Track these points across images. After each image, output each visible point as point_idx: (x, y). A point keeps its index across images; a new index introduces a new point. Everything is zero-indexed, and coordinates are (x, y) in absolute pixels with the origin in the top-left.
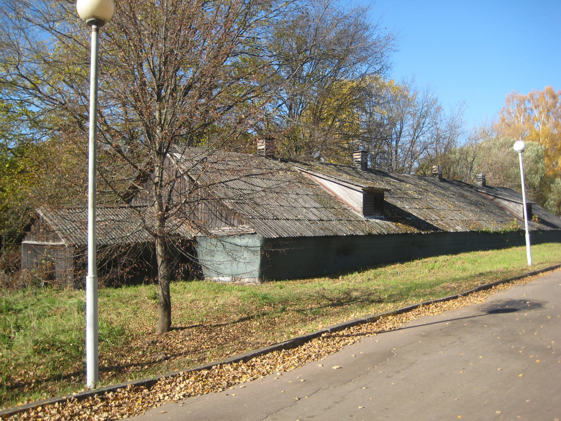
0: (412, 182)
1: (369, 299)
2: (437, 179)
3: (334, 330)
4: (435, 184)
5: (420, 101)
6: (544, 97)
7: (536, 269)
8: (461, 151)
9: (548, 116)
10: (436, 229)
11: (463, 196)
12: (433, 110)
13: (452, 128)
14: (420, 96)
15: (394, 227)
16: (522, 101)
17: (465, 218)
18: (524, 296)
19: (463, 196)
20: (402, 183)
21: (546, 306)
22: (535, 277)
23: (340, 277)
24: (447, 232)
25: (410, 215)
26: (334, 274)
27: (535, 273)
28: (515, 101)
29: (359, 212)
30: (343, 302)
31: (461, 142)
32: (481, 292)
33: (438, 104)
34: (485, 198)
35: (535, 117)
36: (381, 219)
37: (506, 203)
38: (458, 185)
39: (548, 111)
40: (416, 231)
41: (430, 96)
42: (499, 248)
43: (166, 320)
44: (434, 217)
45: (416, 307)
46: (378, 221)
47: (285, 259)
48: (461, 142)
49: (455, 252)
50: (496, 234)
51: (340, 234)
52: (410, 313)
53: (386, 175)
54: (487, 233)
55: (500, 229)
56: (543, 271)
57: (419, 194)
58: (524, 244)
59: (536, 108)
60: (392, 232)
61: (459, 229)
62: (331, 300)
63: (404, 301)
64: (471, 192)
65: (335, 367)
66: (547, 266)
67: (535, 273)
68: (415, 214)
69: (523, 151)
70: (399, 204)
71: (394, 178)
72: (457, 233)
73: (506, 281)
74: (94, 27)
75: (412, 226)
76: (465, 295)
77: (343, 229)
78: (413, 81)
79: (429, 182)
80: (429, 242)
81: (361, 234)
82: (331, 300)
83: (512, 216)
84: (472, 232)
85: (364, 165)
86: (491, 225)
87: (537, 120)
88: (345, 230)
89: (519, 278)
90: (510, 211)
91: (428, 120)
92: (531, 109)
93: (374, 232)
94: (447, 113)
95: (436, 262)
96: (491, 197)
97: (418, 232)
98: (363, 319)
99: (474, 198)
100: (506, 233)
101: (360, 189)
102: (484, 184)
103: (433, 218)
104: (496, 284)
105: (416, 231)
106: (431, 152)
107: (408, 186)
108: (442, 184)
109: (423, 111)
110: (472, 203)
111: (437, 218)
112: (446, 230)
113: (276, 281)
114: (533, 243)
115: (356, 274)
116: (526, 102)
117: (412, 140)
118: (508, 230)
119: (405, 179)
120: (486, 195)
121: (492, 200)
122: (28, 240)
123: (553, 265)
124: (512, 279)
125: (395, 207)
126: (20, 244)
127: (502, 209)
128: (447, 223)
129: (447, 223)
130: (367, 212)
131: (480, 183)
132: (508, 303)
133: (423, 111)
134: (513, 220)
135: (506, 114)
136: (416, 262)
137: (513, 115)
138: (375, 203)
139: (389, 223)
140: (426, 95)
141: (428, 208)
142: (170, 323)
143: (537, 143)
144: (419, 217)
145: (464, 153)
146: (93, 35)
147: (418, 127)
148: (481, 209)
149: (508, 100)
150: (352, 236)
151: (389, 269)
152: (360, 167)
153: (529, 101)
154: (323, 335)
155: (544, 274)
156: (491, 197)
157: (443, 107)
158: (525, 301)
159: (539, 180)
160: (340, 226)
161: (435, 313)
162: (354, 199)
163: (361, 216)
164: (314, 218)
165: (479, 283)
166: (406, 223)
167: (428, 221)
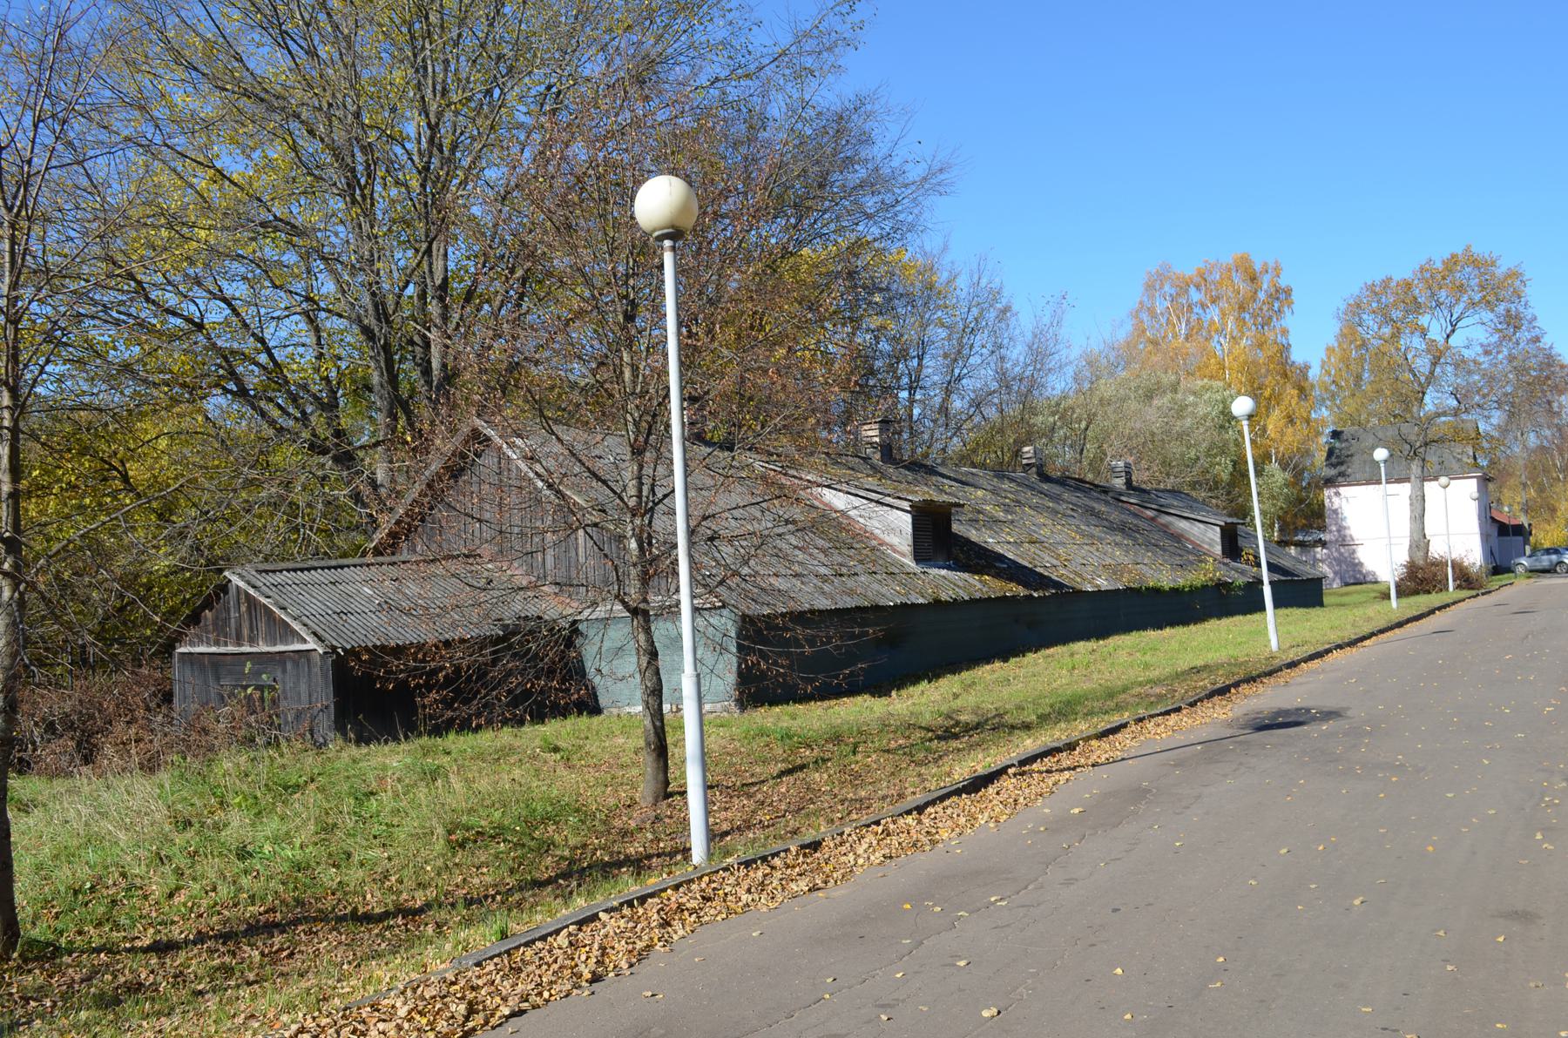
0: (985, 484)
1: (995, 726)
2: (1034, 477)
3: (1023, 763)
4: (1033, 489)
5: (963, 295)
6: (1230, 278)
7: (1292, 656)
8: (1055, 408)
9: (1241, 321)
10: (1058, 585)
11: (1097, 515)
12: (992, 315)
13: (1039, 355)
14: (962, 282)
15: (979, 586)
16: (1183, 286)
17: (1109, 561)
18: (1298, 702)
19: (1097, 515)
20: (967, 488)
21: (1349, 713)
22: (1294, 672)
23: (894, 693)
24: (1081, 591)
25: (1001, 558)
26: (879, 686)
27: (1293, 665)
28: (1167, 288)
29: (904, 555)
30: (951, 732)
31: (1057, 385)
32: (1216, 699)
33: (1004, 301)
34: (1136, 515)
35: (1212, 322)
36: (949, 568)
37: (1183, 524)
38: (1077, 489)
39: (1242, 308)
40: (1022, 591)
41: (984, 282)
42: (1185, 622)
43: (661, 776)
44: (1048, 560)
45: (1124, 726)
46: (944, 572)
47: (786, 658)
48: (1057, 385)
49: (1102, 634)
50: (1175, 591)
51: (883, 602)
52: (1119, 736)
53: (931, 471)
54: (1157, 591)
55: (1181, 582)
56: (1306, 660)
57: (1007, 512)
58: (1262, 608)
59: (1213, 302)
60: (978, 595)
61: (1103, 583)
62: (928, 730)
63: (1115, 712)
64: (1107, 503)
65: (1076, 811)
66: (1312, 651)
67: (1293, 665)
68: (1010, 556)
69: (1250, 417)
70: (973, 535)
71: (949, 478)
72: (1100, 594)
73: (1250, 680)
74: (667, 243)
75: (1011, 580)
76: (1193, 704)
77: (884, 590)
78: (945, 248)
79: (1019, 484)
80: (1047, 615)
81: (921, 601)
82: (928, 730)
83: (1199, 554)
84: (1129, 590)
85: (887, 451)
86: (1164, 576)
87: (1217, 331)
88: (890, 594)
89: (1270, 674)
90: (1192, 542)
91: (979, 339)
92: (1203, 306)
93: (944, 597)
94: (1024, 322)
95: (1072, 655)
96: (1150, 513)
97: (1027, 592)
98: (1056, 745)
99: (1115, 516)
100: (1194, 591)
101: (906, 505)
102: (1129, 483)
103: (1043, 563)
104: (1237, 685)
105: (1022, 591)
106: (991, 412)
107: (980, 493)
108: (1045, 486)
109: (971, 318)
110: (1112, 528)
111: (1055, 562)
112: (1078, 587)
113: (771, 705)
114: (1278, 604)
115: (924, 685)
116: (1192, 290)
117: (950, 388)
118: (1198, 583)
119: (970, 479)
120: (1133, 506)
121: (1153, 519)
122: (192, 644)
123: (1321, 648)
124: (1259, 676)
125: (968, 541)
126: (171, 655)
127: (1178, 538)
128: (1075, 573)
129: (1075, 573)
130: (920, 555)
131: (1119, 483)
132: (1280, 713)
133: (971, 318)
134: (1205, 562)
135: (1145, 317)
136: (1030, 656)
137: (1163, 321)
138: (936, 535)
139: (966, 575)
140: (975, 279)
141: (1032, 542)
142: (667, 783)
143: (1221, 384)
144: (1020, 561)
145: (1063, 412)
146: (668, 259)
147: (957, 356)
148: (1135, 539)
149: (1150, 287)
150: (904, 605)
151: (915, 690)
152: (878, 456)
153: (1198, 287)
154: (1011, 771)
155: (1310, 664)
156: (1150, 513)
157: (1015, 308)
158: (1308, 711)
159: (1230, 468)
160: (876, 586)
161: (1160, 732)
162: (893, 527)
163: (909, 562)
164: (823, 570)
165: (1206, 683)
166: (998, 575)
167: (1038, 569)
